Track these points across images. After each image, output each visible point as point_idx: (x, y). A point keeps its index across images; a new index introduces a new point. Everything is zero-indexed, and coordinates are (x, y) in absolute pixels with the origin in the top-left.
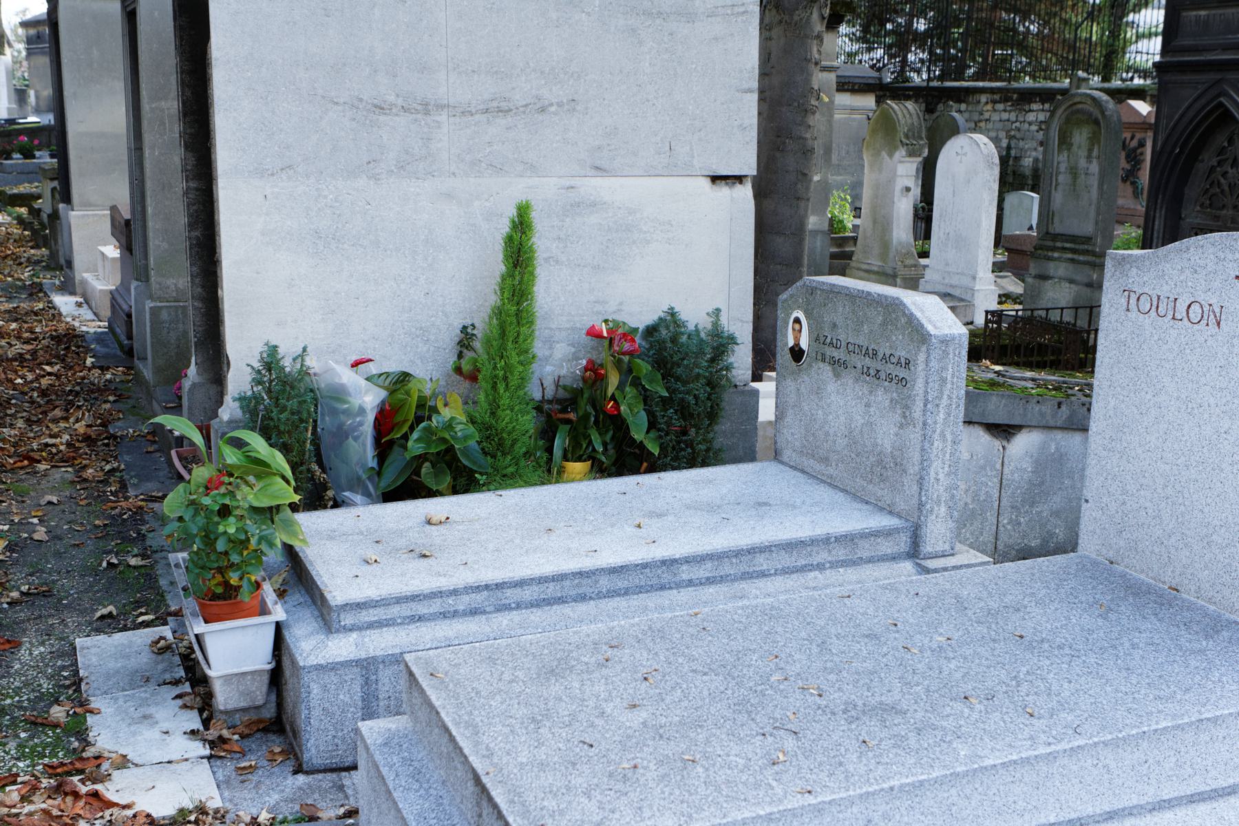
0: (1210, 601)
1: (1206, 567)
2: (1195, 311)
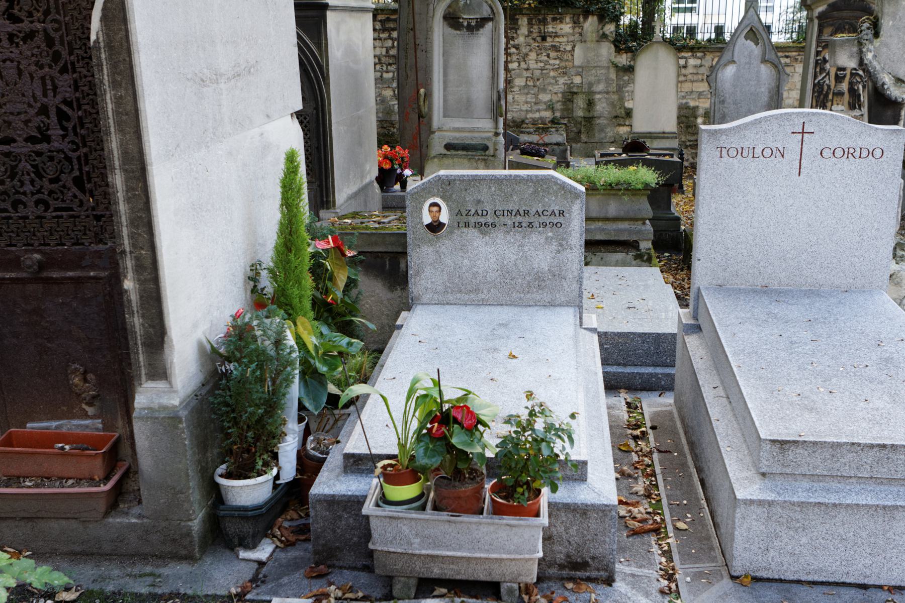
0: (787, 285)
1: (784, 270)
2: (767, 152)
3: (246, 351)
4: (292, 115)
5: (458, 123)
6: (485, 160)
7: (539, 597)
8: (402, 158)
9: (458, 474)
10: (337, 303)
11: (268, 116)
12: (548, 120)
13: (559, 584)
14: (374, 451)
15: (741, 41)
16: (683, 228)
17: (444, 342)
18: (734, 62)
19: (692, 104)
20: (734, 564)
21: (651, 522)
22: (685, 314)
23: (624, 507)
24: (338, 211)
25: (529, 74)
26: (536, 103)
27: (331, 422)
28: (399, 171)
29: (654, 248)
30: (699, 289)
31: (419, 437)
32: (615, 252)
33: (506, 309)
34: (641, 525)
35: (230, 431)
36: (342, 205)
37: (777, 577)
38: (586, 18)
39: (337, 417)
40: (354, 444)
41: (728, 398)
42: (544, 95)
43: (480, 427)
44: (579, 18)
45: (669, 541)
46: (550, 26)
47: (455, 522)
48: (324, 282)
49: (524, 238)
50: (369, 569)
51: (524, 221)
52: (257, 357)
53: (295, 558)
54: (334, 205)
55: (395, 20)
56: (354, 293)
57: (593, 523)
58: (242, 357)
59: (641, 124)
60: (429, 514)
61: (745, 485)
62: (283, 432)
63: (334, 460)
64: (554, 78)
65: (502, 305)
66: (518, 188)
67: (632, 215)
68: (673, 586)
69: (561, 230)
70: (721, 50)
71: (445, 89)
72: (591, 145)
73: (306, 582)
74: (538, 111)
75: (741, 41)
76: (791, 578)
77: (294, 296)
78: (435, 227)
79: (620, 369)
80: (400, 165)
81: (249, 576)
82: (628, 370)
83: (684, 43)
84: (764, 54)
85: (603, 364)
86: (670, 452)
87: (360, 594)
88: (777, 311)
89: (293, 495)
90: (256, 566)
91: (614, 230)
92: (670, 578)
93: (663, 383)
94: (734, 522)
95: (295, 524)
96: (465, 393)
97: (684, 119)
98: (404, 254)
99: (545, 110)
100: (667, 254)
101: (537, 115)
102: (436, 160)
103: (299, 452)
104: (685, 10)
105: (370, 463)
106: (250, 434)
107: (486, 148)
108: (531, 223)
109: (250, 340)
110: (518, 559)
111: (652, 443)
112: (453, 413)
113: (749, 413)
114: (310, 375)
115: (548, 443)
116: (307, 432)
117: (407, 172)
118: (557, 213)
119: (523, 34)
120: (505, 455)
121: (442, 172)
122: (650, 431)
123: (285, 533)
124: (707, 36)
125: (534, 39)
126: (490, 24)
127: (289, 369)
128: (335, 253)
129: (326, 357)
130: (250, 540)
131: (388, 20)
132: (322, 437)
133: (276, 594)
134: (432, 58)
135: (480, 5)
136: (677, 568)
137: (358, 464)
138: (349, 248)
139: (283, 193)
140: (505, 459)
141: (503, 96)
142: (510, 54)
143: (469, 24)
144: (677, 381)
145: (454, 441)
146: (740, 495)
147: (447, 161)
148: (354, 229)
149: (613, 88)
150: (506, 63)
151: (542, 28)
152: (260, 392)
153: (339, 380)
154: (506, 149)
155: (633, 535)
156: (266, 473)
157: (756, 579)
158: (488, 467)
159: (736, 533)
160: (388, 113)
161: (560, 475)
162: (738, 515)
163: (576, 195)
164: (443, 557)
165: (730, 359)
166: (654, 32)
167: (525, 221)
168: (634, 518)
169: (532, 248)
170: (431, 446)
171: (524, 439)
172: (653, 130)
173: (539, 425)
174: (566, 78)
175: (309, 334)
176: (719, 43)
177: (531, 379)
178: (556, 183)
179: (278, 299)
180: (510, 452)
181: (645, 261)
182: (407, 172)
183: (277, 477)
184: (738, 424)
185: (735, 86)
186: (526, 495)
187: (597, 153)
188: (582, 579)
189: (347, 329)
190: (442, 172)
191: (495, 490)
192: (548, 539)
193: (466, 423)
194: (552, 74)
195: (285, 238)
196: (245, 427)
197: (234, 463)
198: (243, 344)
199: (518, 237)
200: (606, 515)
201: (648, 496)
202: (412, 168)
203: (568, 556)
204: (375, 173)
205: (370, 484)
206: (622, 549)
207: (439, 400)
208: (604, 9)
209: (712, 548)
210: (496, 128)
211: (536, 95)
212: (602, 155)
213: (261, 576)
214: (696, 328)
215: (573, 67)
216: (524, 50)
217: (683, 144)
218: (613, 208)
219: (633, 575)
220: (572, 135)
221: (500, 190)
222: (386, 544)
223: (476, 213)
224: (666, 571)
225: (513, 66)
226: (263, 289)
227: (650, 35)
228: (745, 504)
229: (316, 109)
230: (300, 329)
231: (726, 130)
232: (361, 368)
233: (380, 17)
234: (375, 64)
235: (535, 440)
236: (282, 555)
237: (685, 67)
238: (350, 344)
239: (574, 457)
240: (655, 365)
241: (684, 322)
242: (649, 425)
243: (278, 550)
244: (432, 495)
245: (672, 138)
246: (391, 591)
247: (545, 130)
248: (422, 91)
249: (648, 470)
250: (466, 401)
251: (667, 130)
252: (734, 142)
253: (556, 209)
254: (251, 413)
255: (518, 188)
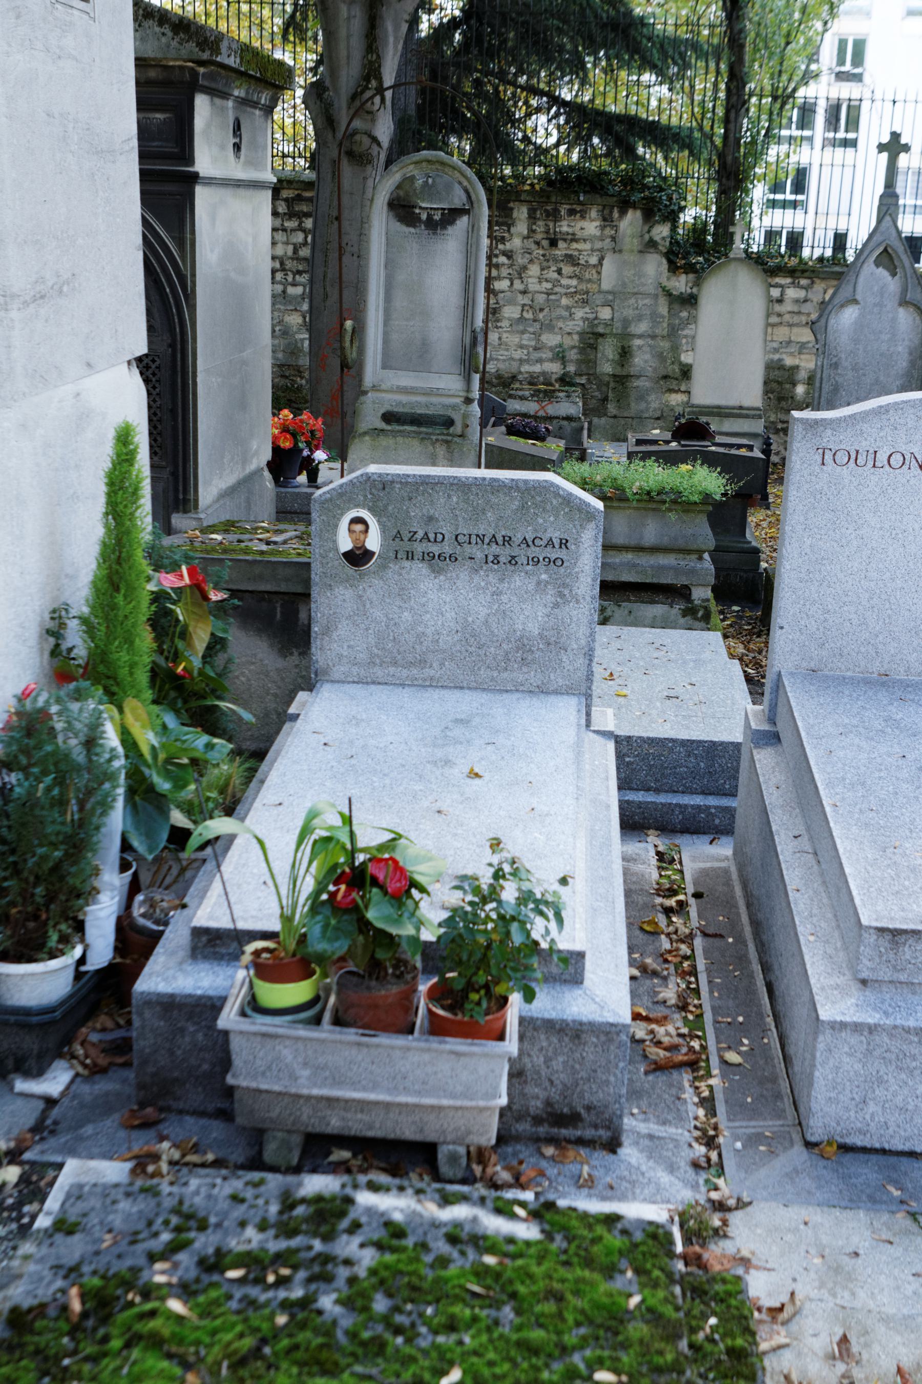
1: (915, 650)
2: (897, 460)
3: (37, 755)
4: (129, 362)
5: (406, 380)
6: (447, 442)
7: (498, 1168)
8: (312, 432)
9: (375, 969)
10: (192, 679)
11: (89, 365)
12: (554, 377)
13: (532, 1148)
14: (242, 925)
15: (869, 268)
16: (764, 565)
17: (364, 747)
18: (855, 301)
19: (789, 361)
20: (811, 1123)
21: (684, 1050)
22: (756, 714)
23: (643, 1024)
24: (202, 516)
25: (526, 300)
26: (536, 349)
27: (175, 871)
28: (306, 453)
29: (717, 598)
30: (779, 675)
31: (315, 906)
32: (652, 602)
33: (468, 695)
34: (668, 1054)
35: (6, 884)
36: (209, 507)
37: (877, 1146)
38: (623, 213)
39: (184, 863)
40: (209, 912)
41: (816, 854)
42: (551, 336)
43: (414, 892)
44: (611, 212)
45: (712, 1082)
46: (564, 223)
47: (367, 1046)
48: (172, 641)
49: (502, 580)
50: (226, 1115)
51: (503, 553)
52: (56, 764)
53: (107, 1094)
54: (196, 506)
55: (310, 200)
56: (220, 660)
57: (590, 1052)
58: (30, 765)
59: (705, 392)
60: (326, 1031)
61: (831, 994)
62: (94, 888)
63: (176, 936)
64: (568, 308)
65: (462, 688)
66: (494, 500)
67: (681, 543)
68: (714, 1156)
69: (562, 570)
70: (839, 276)
71: (386, 323)
72: (622, 422)
73: (122, 1134)
74: (540, 361)
75: (869, 268)
76: (900, 1147)
77: (121, 663)
78: (358, 557)
79: (650, 798)
80: (308, 444)
81: (30, 1122)
82: (662, 799)
83: (781, 263)
84: (904, 290)
85: (620, 788)
86: (721, 936)
87: (210, 1157)
88: (900, 715)
89: (107, 989)
90: (41, 1105)
91: (652, 567)
92: (710, 1142)
93: (717, 821)
94: (814, 1057)
95: (109, 1036)
96: (392, 836)
97: (774, 385)
98: (306, 596)
99: (552, 360)
100: (736, 608)
101: (537, 368)
102: (367, 438)
103: (119, 921)
104: (784, 205)
105: (235, 945)
106: (39, 890)
107: (450, 423)
108: (513, 557)
109: (45, 737)
110: (467, 1108)
111: (695, 921)
112: (371, 869)
113: (847, 882)
114: (141, 793)
115: (523, 923)
116: (134, 888)
117: (320, 455)
118: (556, 542)
119: (519, 234)
120: (453, 941)
121: (373, 468)
122: (692, 901)
123: (93, 1052)
124: (817, 253)
125: (538, 243)
126: (465, 219)
127: (107, 786)
128: (192, 593)
129: (170, 767)
130: (32, 1062)
131: (299, 198)
132: (158, 897)
133: (73, 1152)
134: (367, 266)
135: (449, 188)
136: (721, 1126)
137: (214, 944)
138: (217, 587)
139: (109, 495)
140: (453, 946)
141: (480, 338)
142: (497, 266)
143: (430, 217)
144: (739, 822)
145: (371, 915)
146: (826, 1013)
147: (384, 441)
148: (225, 551)
149: (663, 329)
150: (489, 280)
151: (551, 225)
152: (55, 824)
153: (190, 803)
154: (483, 424)
155: (655, 1070)
156: (63, 954)
157: (845, 1148)
158: (425, 957)
159: (817, 1074)
160: (292, 353)
161: (539, 975)
162: (821, 1046)
163: (588, 514)
164: (347, 1101)
165: (822, 793)
166: (732, 242)
167: (504, 553)
168: (658, 1043)
169: (514, 599)
170: (333, 922)
171: (483, 915)
172: (722, 402)
173: (509, 893)
174: (587, 310)
175: (143, 727)
176: (835, 268)
177: (502, 813)
178: (557, 495)
179: (94, 668)
180: (460, 936)
181: (699, 620)
182: (320, 455)
183: (82, 961)
184: (830, 898)
185: (856, 341)
186: (484, 1004)
187: (632, 438)
188: (569, 1141)
189: (207, 720)
190: (373, 468)
191: (435, 995)
192: (517, 1075)
193: (392, 886)
194: (564, 301)
195: (110, 568)
196: (32, 879)
197: (11, 937)
198: (32, 742)
199: (492, 578)
200: (611, 1040)
201: (683, 1007)
202: (328, 448)
203: (548, 1103)
204: (267, 455)
205: (232, 977)
206: (635, 1094)
207: (349, 846)
208: (653, 199)
209: (778, 1096)
210: (468, 390)
211: (537, 335)
212: (639, 442)
213: (49, 1122)
214: (772, 738)
215: (600, 292)
216: (521, 260)
217: (772, 427)
218: (651, 531)
219: (651, 1137)
220: (593, 403)
221: (466, 501)
222: (254, 1077)
223: (426, 537)
224: (704, 1131)
225: (502, 285)
226: (70, 650)
227: (725, 246)
228: (833, 1028)
229: (172, 346)
230: (130, 719)
231: (832, 421)
232: (227, 785)
233: (285, 194)
234: (274, 272)
235: (502, 917)
236: (85, 1089)
237: (780, 301)
238: (209, 746)
239: (562, 945)
240: (705, 793)
241: (754, 726)
242: (690, 890)
243: (79, 1079)
244: (332, 1000)
245: (753, 417)
246: (260, 1153)
247: (549, 395)
248: (349, 324)
249: (686, 964)
250: (393, 849)
251: (747, 403)
252: (846, 441)
253: (556, 536)
254: (41, 857)
255: (494, 500)
